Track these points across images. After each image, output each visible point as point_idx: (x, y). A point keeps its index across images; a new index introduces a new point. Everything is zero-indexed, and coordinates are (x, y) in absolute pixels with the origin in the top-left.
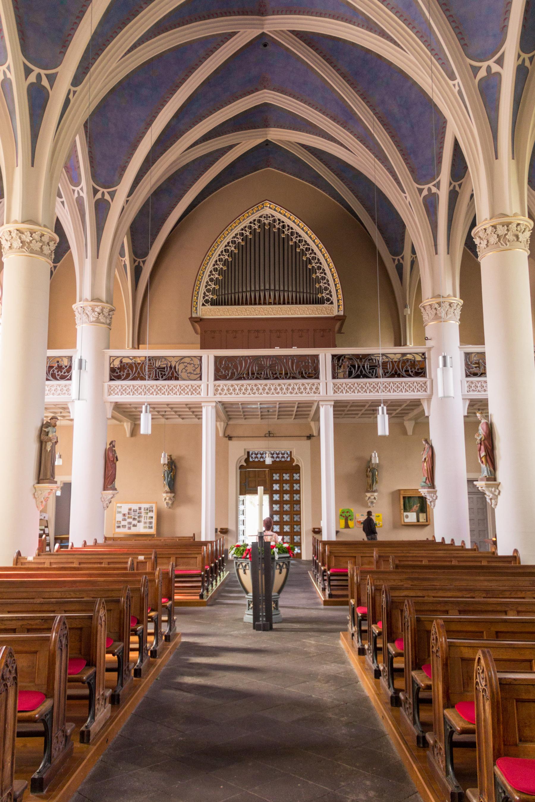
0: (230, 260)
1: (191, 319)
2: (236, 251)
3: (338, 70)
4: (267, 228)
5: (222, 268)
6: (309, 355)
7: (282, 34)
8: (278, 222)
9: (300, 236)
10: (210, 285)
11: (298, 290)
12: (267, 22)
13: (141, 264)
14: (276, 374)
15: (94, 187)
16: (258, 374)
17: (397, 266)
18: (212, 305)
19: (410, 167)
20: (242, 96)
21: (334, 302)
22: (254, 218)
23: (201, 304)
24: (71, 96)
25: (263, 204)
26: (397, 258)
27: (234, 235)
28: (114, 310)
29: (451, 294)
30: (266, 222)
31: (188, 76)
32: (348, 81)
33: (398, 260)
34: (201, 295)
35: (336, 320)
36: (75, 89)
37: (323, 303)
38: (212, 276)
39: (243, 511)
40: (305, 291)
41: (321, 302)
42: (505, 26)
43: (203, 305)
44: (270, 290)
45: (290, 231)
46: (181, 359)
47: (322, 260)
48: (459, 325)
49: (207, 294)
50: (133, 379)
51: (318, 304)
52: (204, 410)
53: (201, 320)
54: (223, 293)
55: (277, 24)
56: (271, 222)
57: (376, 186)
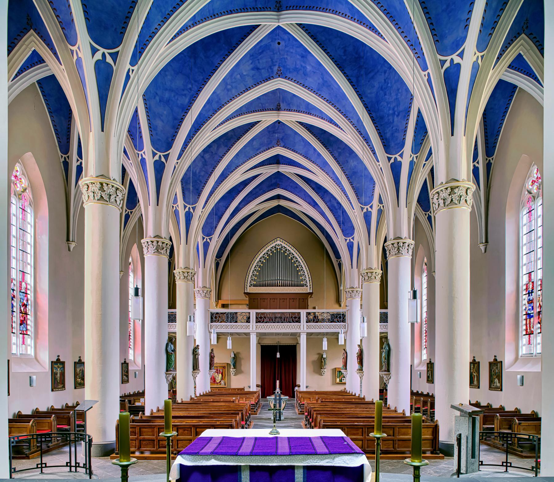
1: (245, 293)
3: (311, 187)
4: (279, 250)
7: (292, 26)
12: (281, 115)
15: (153, 151)
20: (268, 192)
24: (130, 73)
29: (407, 237)
30: (279, 248)
31: (244, 188)
32: (315, 191)
36: (133, 68)
39: (363, 322)
41: (302, 286)
42: (467, 25)
48: (470, 212)
50: (221, 322)
52: (251, 336)
55: (290, 20)
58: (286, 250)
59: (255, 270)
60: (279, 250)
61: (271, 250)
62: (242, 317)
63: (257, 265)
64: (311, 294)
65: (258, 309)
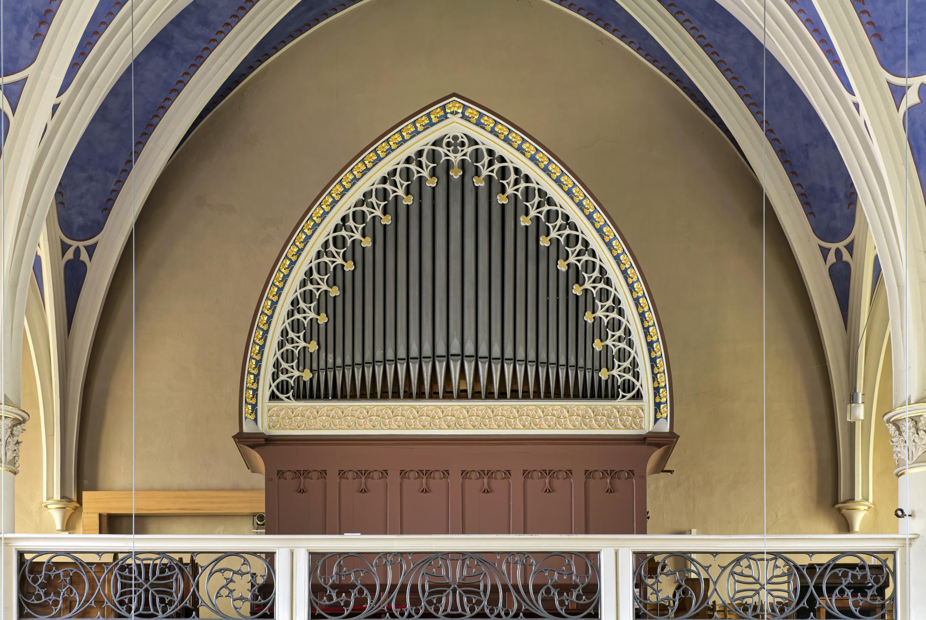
0: (349, 267)
1: (242, 439)
2: (367, 243)
4: (456, 174)
5: (326, 291)
6: (570, 553)
8: (486, 159)
9: (550, 201)
10: (293, 341)
11: (543, 357)
13: (84, 256)
14: (479, 602)
15: (62, 242)
16: (430, 603)
17: (832, 269)
18: (297, 397)
19: (870, 23)
21: (644, 392)
22: (417, 147)
23: (268, 394)
25: (444, 107)
26: (833, 246)
27: (359, 196)
28: (24, 421)
30: (455, 158)
33: (838, 252)
34: (267, 369)
35: (649, 444)
37: (614, 397)
38: (297, 316)
40: (562, 361)
41: (606, 391)
43: (273, 397)
44: (462, 356)
45: (522, 185)
46: (218, 560)
47: (614, 273)
49: (284, 365)
51: (600, 397)
53: (270, 441)
54: (330, 364)
56: (467, 158)
57: (773, 61)
58: (503, 173)
59: (308, 297)
60: (456, 174)
61: (407, 174)
62: (219, 580)
63: (322, 268)
64: (663, 442)
65: (324, 530)
